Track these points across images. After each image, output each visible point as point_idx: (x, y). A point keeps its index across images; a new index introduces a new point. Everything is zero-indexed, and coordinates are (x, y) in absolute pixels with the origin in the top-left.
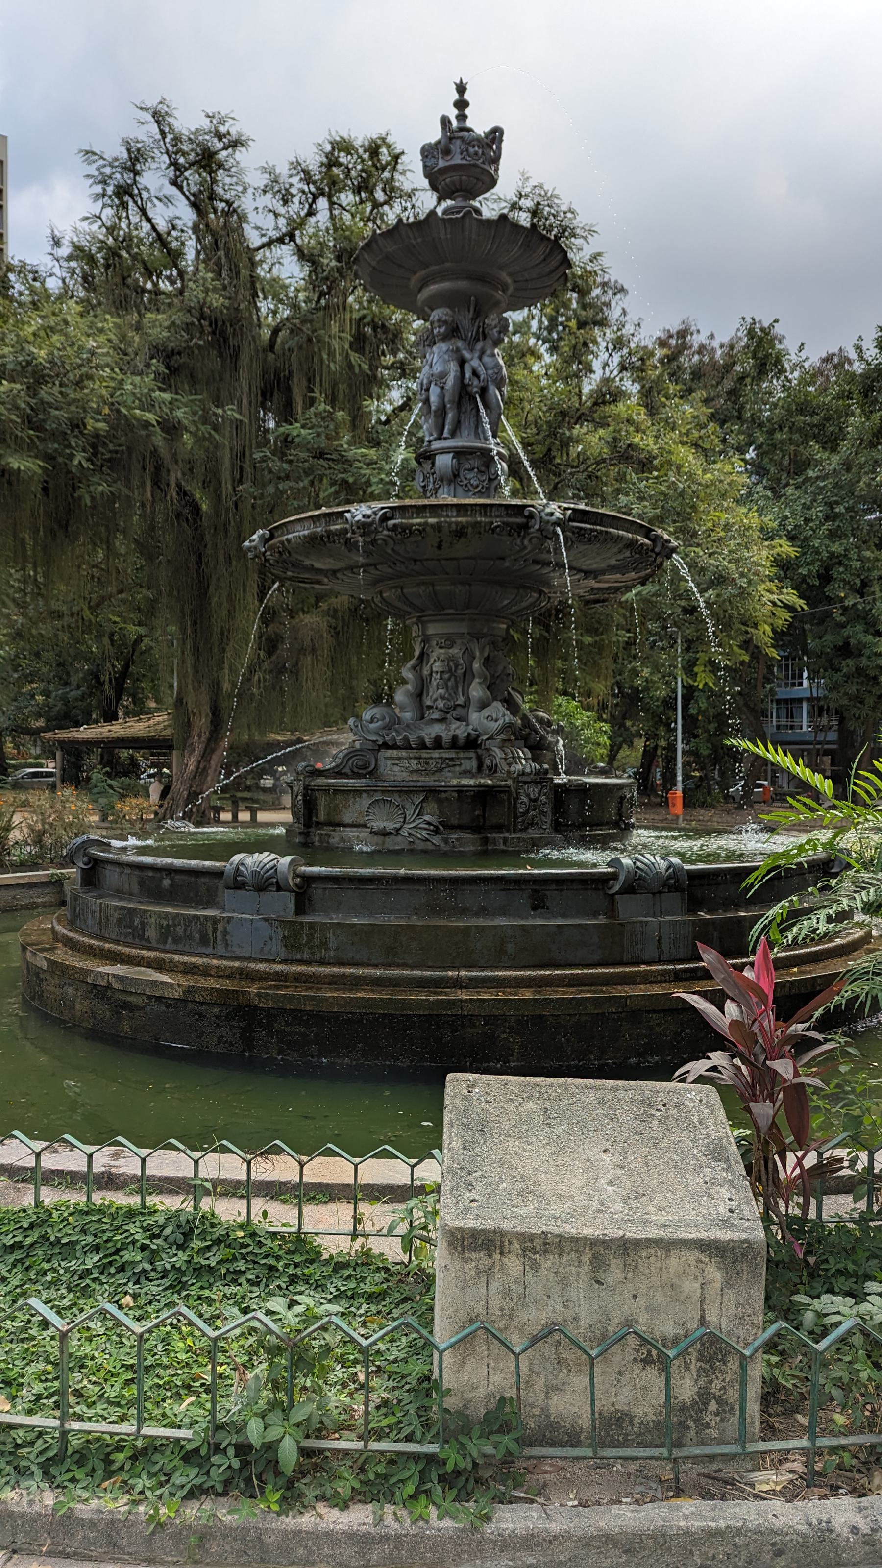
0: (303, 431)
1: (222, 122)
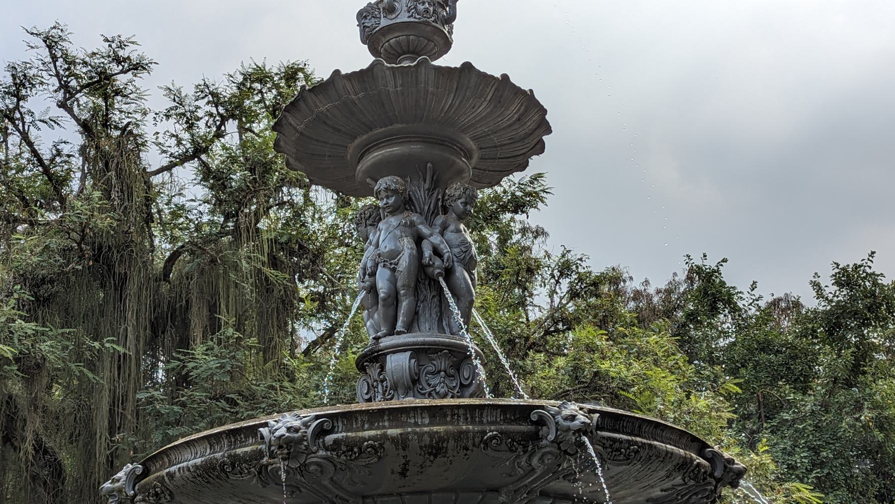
1: (122, 45)
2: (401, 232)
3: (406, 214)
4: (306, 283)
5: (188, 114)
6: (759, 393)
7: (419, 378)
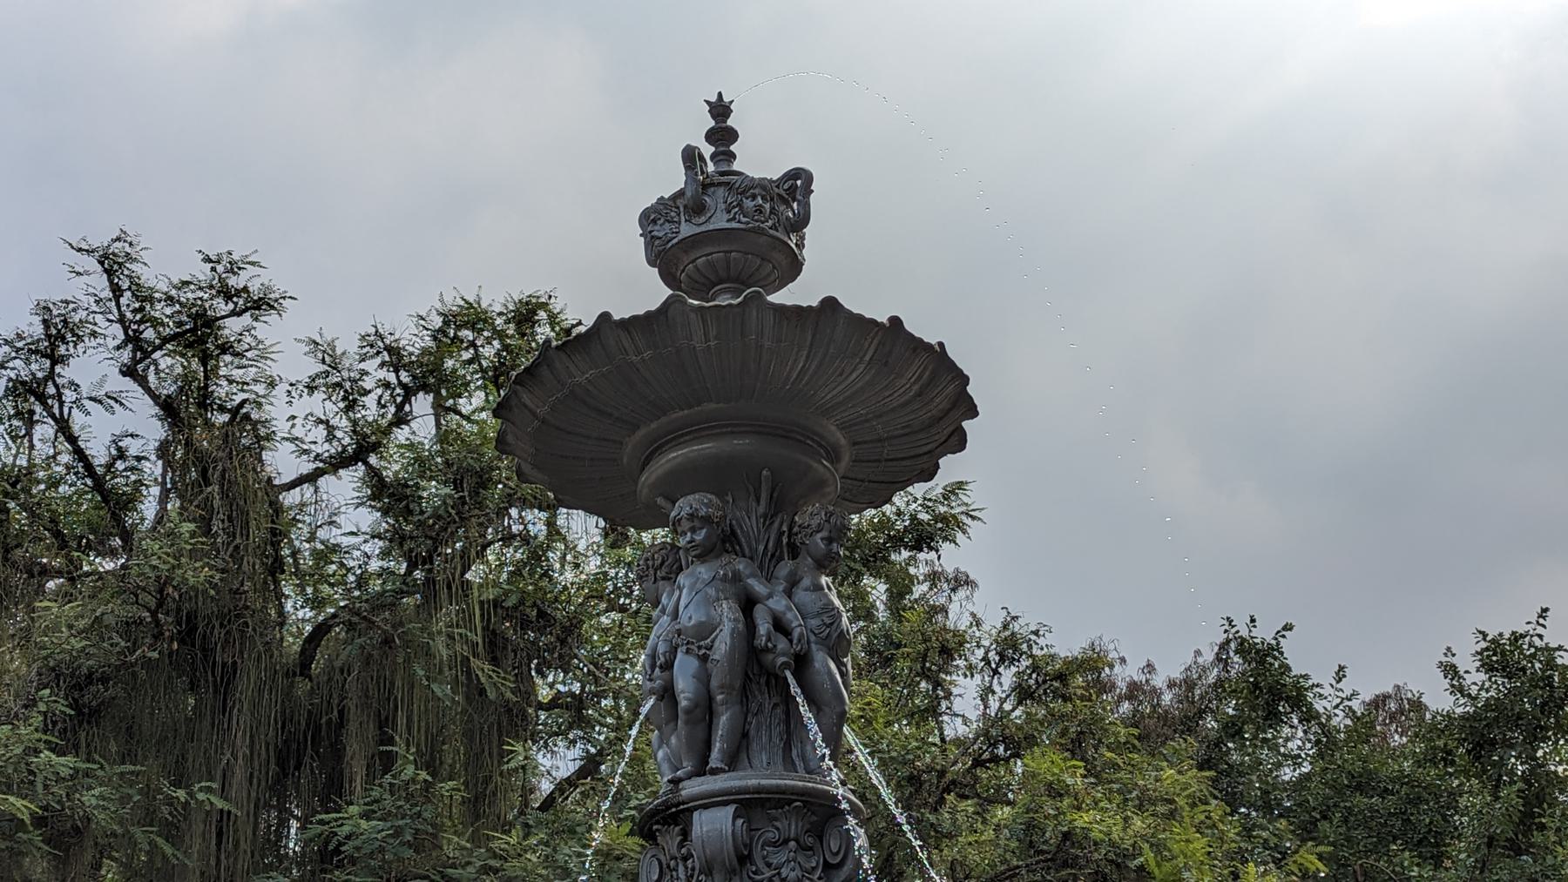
0: (364, 824)
1: (234, 268)
2: (717, 591)
3: (725, 559)
4: (550, 679)
5: (348, 385)
6: (1357, 868)
7: (751, 851)
